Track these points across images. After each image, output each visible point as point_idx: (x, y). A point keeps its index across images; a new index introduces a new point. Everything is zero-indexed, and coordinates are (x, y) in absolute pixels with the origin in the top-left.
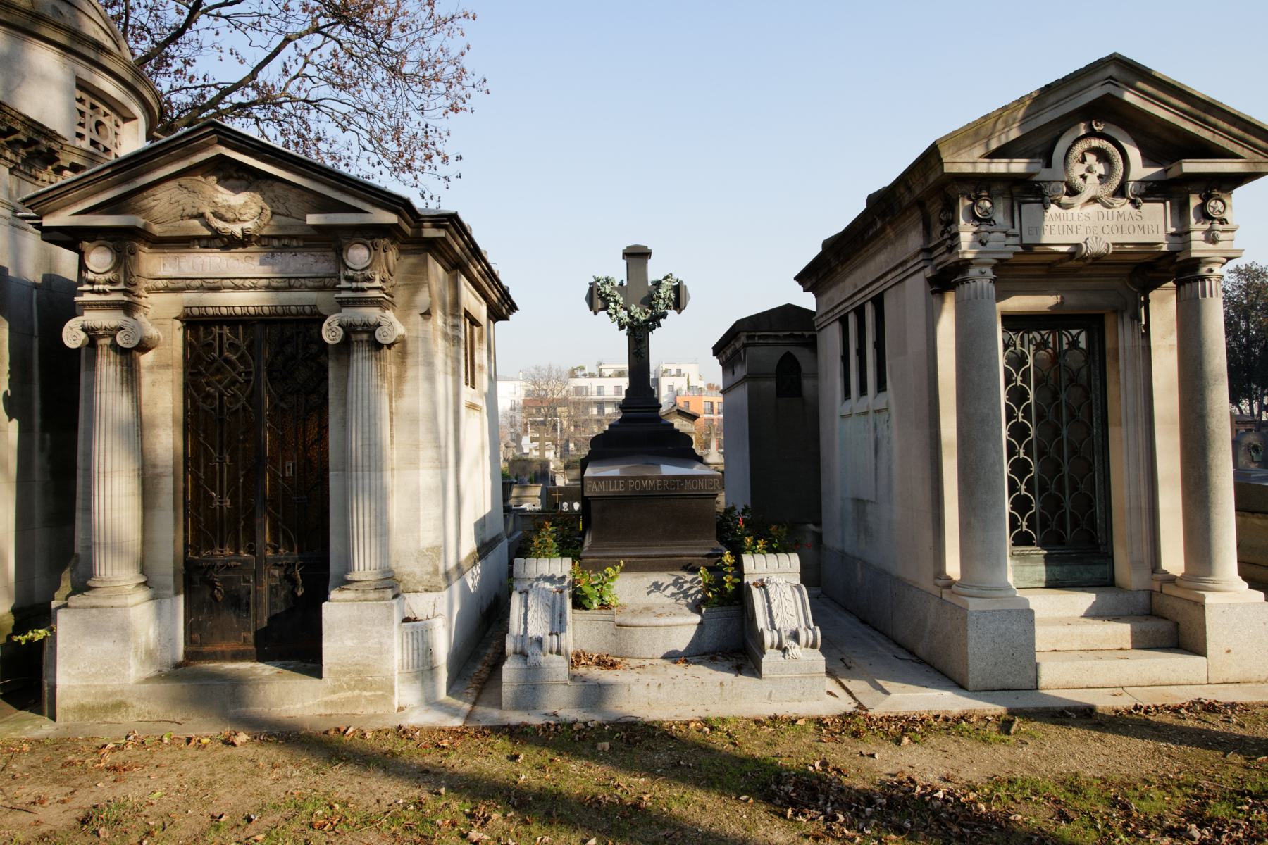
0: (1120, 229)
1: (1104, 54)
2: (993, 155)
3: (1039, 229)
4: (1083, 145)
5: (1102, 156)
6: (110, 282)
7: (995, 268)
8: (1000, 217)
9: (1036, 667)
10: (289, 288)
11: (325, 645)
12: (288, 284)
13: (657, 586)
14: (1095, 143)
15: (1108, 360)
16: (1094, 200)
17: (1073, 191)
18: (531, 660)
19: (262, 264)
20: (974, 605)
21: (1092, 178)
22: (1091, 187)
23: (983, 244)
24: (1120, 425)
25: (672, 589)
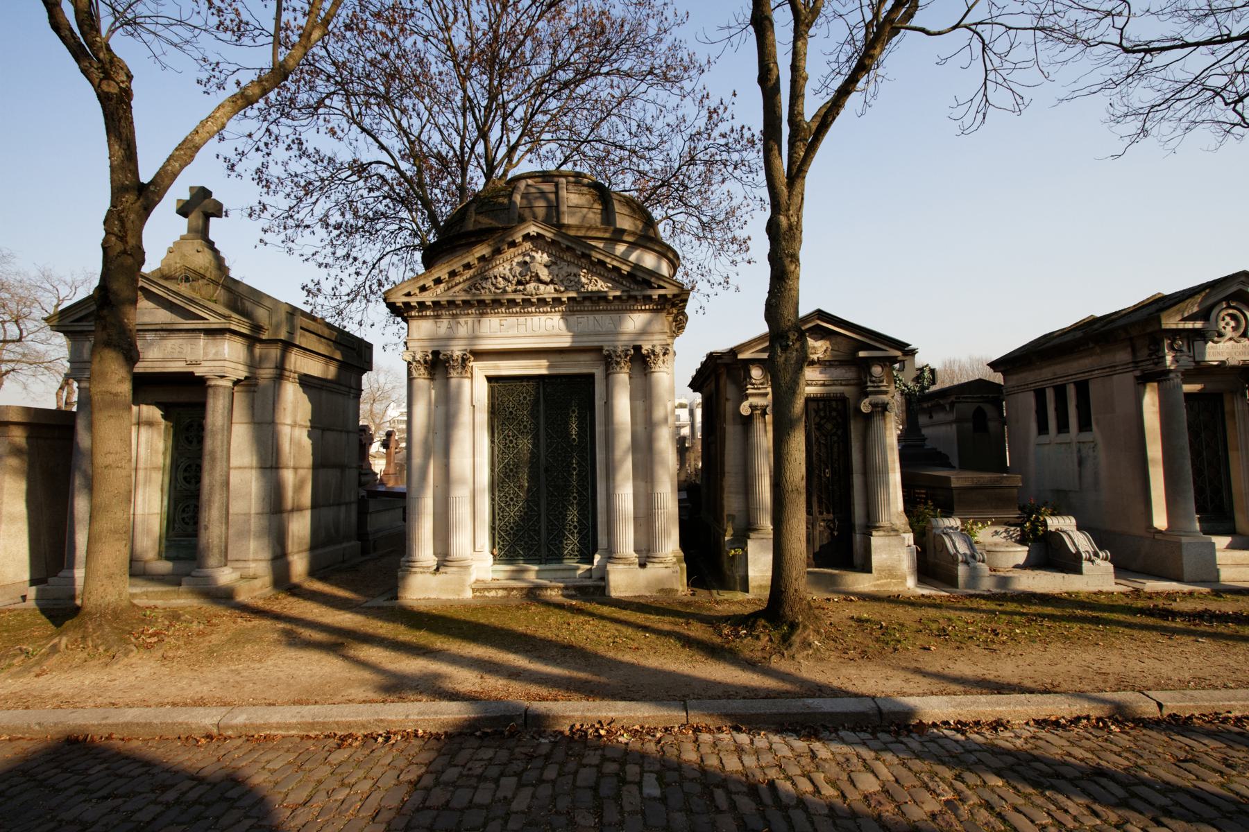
0: (1244, 353)
1: (1241, 270)
2: (1184, 319)
3: (1203, 354)
4: (1225, 312)
5: (1233, 317)
6: (762, 384)
7: (1183, 374)
8: (1185, 349)
9: (1218, 571)
10: (834, 385)
11: (873, 557)
12: (834, 383)
13: (996, 533)
14: (1231, 311)
15: (1227, 417)
16: (1231, 339)
17: (1221, 335)
18: (972, 565)
19: (821, 373)
20: (1184, 540)
21: (1229, 328)
22: (1229, 332)
23: (1177, 361)
24: (1237, 450)
25: (1004, 534)
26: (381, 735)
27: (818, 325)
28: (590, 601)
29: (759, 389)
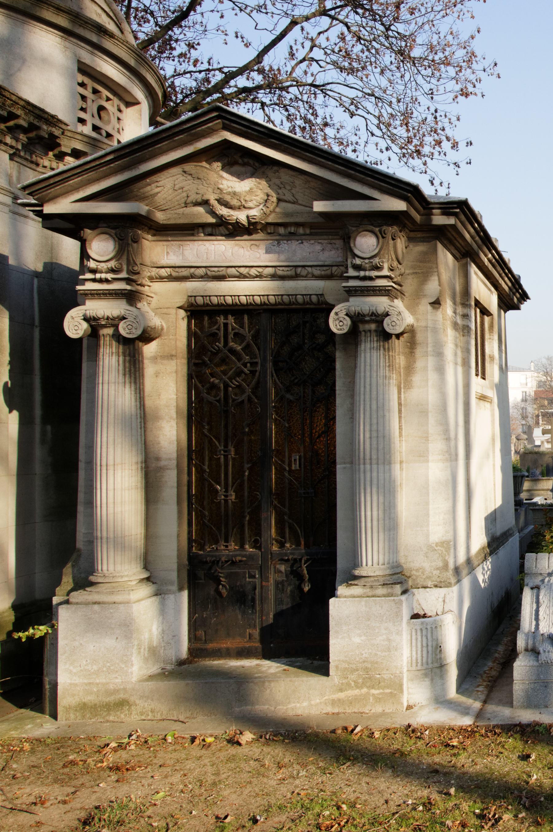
6: (112, 271)
10: (296, 277)
19: (268, 252)
26: (371, 805)
27: (226, 143)
28: (50, 704)
29: (107, 281)
